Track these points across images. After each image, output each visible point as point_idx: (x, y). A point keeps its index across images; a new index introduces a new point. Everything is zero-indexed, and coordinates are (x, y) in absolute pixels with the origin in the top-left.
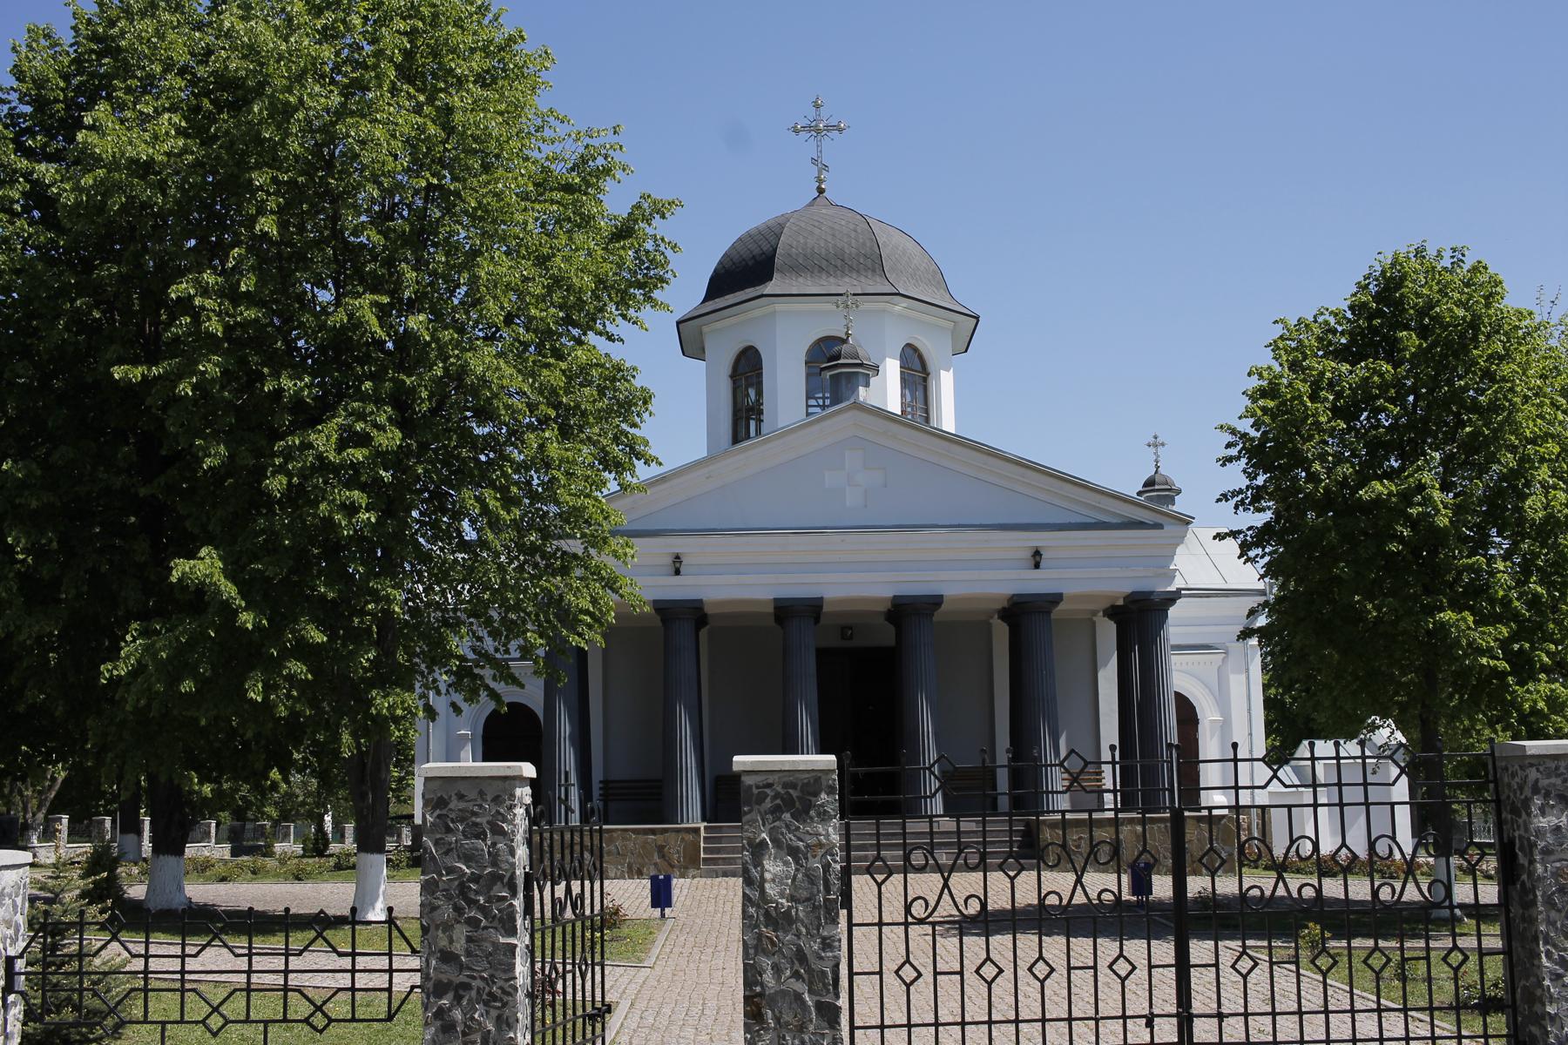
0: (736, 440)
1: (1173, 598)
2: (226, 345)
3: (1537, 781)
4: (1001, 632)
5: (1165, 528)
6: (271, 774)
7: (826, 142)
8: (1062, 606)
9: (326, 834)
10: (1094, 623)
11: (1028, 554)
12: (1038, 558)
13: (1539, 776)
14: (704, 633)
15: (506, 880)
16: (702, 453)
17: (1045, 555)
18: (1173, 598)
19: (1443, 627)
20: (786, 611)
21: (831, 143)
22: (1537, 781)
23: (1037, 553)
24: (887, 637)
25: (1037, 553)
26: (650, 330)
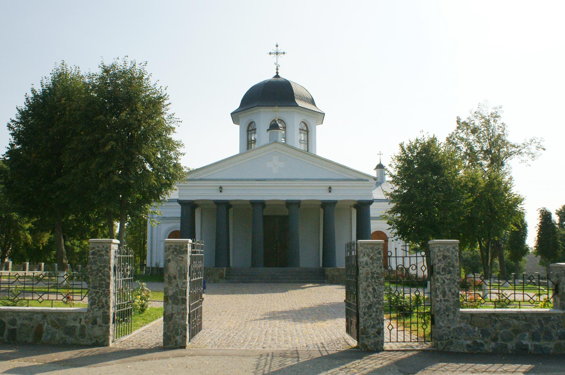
0: (248, 149)
1: (371, 202)
2: (71, 229)
3: (362, 250)
4: (322, 211)
5: (369, 181)
6: (58, 180)
7: (279, 58)
8: (338, 204)
9: (63, 238)
10: (351, 209)
11: (328, 188)
12: (330, 189)
13: (363, 248)
14: (231, 210)
15: (108, 267)
16: (237, 152)
17: (333, 188)
18: (371, 202)
19: (74, 248)
20: (254, 203)
21: (281, 58)
22: (362, 250)
23: (330, 188)
24: (286, 212)
25: (330, 188)
26: (285, 52)
